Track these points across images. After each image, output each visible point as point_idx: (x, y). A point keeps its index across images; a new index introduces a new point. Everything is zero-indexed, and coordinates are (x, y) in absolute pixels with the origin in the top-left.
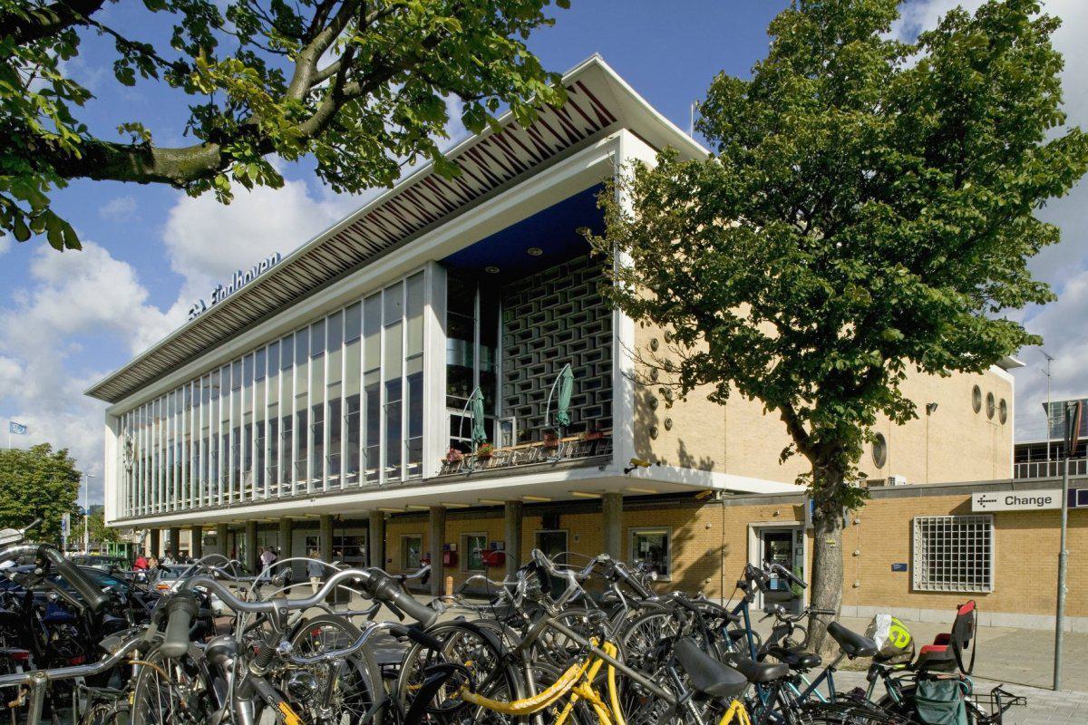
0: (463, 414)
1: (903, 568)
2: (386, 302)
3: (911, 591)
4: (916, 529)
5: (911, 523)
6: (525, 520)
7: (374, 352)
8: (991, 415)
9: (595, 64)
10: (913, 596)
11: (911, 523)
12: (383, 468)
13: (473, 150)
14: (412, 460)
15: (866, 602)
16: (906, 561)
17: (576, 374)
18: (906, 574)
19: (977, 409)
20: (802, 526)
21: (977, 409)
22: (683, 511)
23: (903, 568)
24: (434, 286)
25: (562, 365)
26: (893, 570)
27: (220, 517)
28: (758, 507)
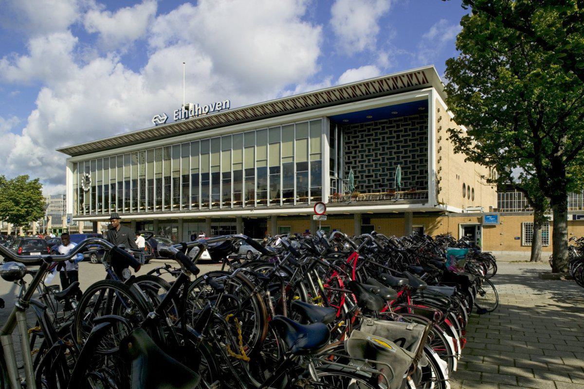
0: (333, 178)
1: (519, 238)
2: (283, 132)
3: (522, 245)
4: (523, 226)
5: (522, 224)
6: (184, 224)
7: (128, 171)
8: (469, 198)
9: (432, 68)
10: (522, 247)
11: (522, 224)
12: (147, 207)
13: (294, 100)
14: (126, 207)
15: (505, 250)
16: (520, 236)
17: (402, 168)
18: (520, 240)
19: (464, 196)
20: (481, 225)
21: (464, 196)
22: (430, 218)
23: (519, 238)
24: (326, 126)
25: (396, 164)
26: (515, 239)
27: (212, 216)
28: (463, 218)
